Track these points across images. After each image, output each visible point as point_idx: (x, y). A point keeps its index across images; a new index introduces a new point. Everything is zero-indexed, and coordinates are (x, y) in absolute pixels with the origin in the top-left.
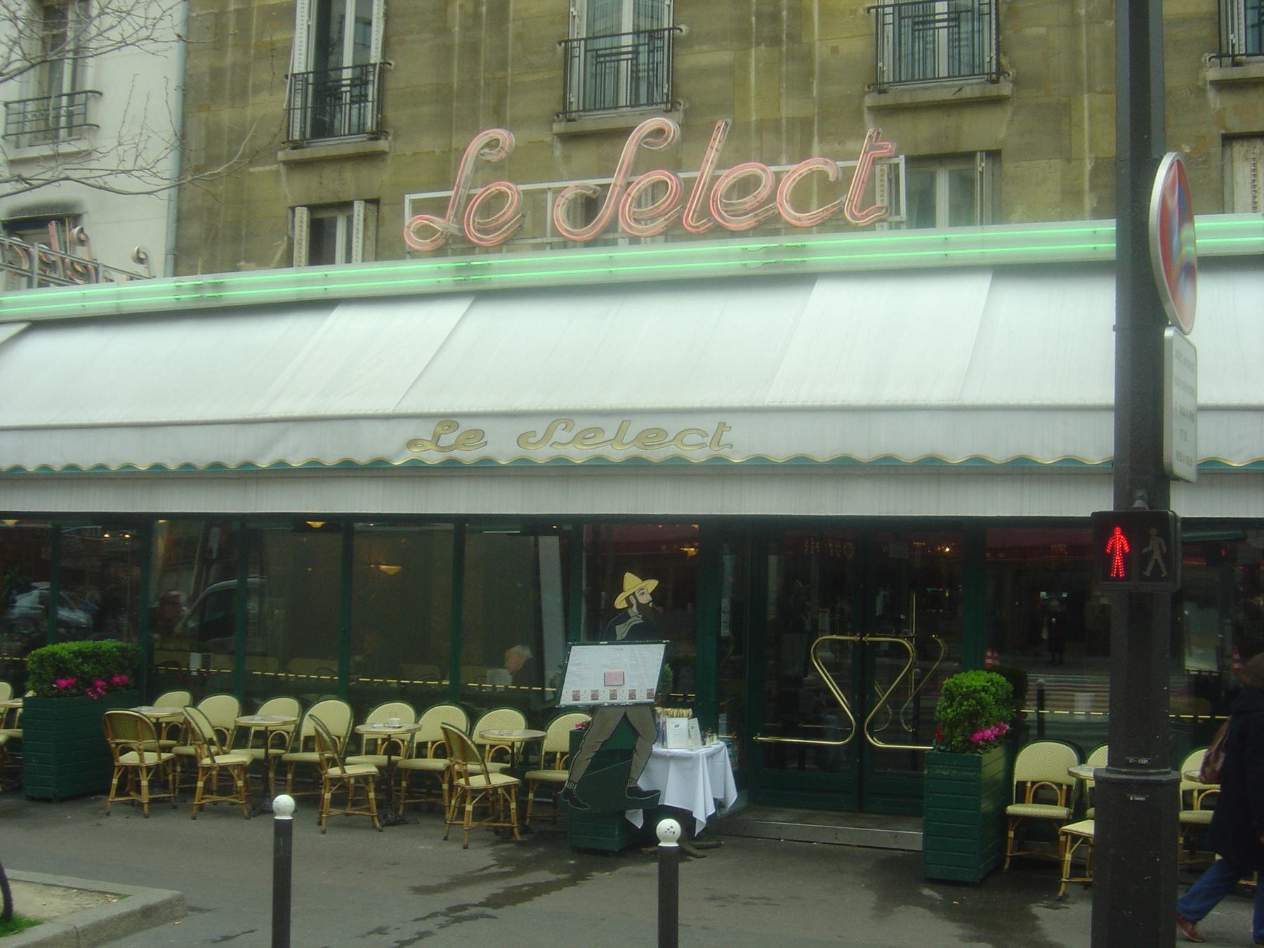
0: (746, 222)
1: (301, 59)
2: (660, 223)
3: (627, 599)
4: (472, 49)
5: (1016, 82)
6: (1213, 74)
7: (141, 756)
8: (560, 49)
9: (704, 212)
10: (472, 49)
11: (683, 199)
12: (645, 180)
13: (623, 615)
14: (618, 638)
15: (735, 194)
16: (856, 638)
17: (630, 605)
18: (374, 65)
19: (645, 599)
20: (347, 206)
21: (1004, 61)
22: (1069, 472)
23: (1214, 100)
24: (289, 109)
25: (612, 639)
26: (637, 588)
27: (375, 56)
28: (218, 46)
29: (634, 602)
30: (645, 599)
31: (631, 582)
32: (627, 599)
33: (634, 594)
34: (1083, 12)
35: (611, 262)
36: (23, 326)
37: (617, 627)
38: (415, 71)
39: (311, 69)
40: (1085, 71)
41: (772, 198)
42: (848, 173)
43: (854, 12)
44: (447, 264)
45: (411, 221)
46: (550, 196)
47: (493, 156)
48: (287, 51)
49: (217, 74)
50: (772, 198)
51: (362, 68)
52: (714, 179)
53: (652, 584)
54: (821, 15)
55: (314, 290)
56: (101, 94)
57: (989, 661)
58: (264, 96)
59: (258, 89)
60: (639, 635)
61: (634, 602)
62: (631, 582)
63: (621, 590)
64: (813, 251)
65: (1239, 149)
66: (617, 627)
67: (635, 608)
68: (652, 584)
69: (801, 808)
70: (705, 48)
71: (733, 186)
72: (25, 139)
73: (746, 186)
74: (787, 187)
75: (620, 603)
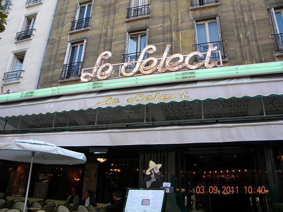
1: (66, 61)
3: (150, 171)
5: (229, 59)
8: (122, 57)
9: (164, 65)
11: (158, 64)
13: (149, 178)
14: (147, 187)
15: (172, 62)
17: (152, 174)
18: (81, 62)
19: (157, 171)
21: (225, 55)
24: (62, 71)
25: (145, 188)
26: (154, 167)
27: (82, 60)
28: (50, 61)
29: (153, 172)
30: (157, 171)
31: (152, 164)
32: (150, 171)
33: (153, 169)
34: (243, 44)
37: (147, 182)
39: (68, 63)
40: (245, 56)
41: (184, 62)
42: (205, 55)
43: (189, 46)
44: (91, 83)
45: (83, 75)
46: (120, 66)
48: (63, 61)
49: (49, 66)
50: (184, 62)
51: (79, 63)
52: (166, 59)
53: (160, 166)
54: (182, 47)
55: (56, 93)
58: (57, 70)
59: (56, 68)
60: (156, 186)
61: (153, 172)
62: (152, 164)
63: (148, 167)
64: (197, 74)
66: (147, 182)
67: (153, 175)
68: (160, 166)
70: (155, 55)
71: (171, 61)
74: (187, 59)
75: (148, 173)
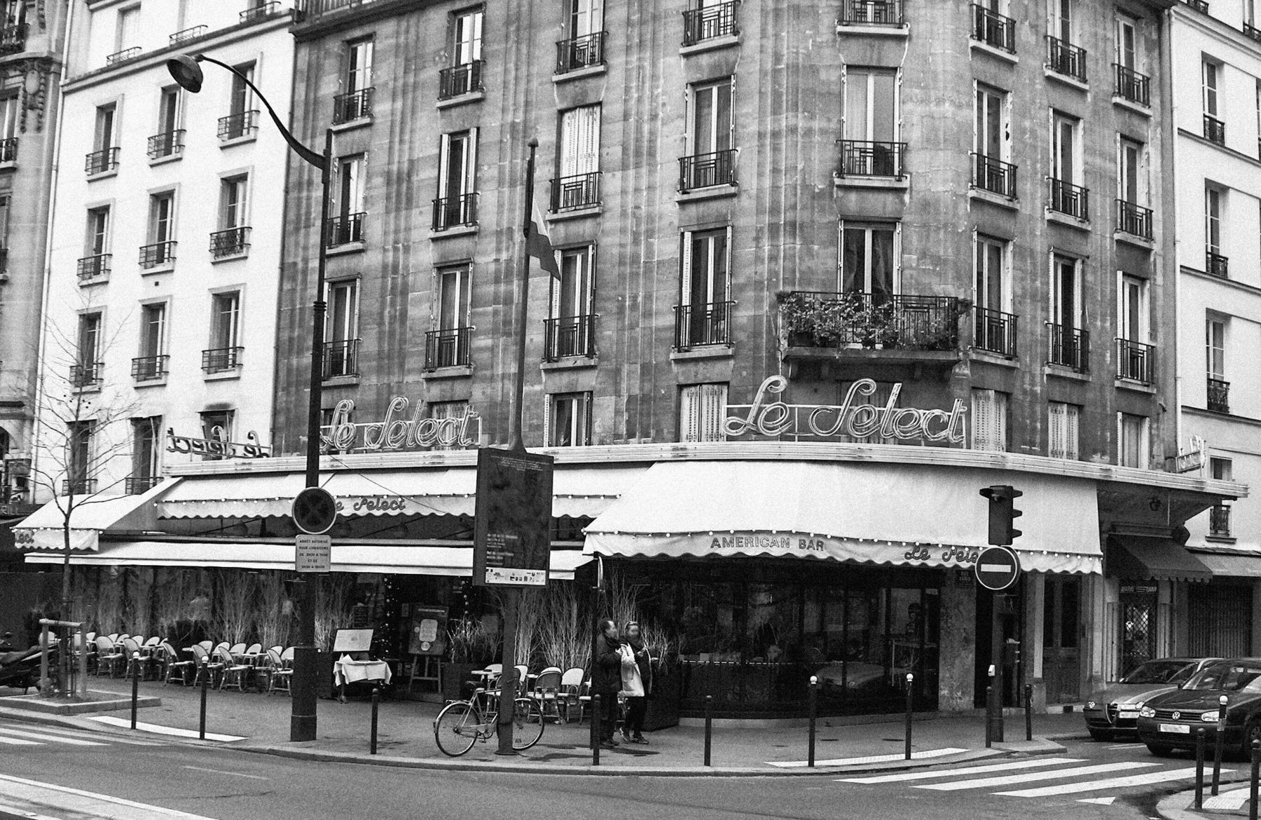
0: (776, 433)
2: (397, 445)
4: (392, 333)
6: (672, 356)
7: (1002, 507)
10: (392, 333)
12: (769, 407)
16: (61, 622)
20: (466, 132)
22: (236, 438)
23: (675, 367)
35: (215, 467)
36: (287, 127)
38: (370, 345)
41: (755, 422)
47: (866, 393)
56: (152, 166)
57: (354, 672)
65: (567, 115)
69: (736, 718)
72: (212, 370)
73: (909, 417)
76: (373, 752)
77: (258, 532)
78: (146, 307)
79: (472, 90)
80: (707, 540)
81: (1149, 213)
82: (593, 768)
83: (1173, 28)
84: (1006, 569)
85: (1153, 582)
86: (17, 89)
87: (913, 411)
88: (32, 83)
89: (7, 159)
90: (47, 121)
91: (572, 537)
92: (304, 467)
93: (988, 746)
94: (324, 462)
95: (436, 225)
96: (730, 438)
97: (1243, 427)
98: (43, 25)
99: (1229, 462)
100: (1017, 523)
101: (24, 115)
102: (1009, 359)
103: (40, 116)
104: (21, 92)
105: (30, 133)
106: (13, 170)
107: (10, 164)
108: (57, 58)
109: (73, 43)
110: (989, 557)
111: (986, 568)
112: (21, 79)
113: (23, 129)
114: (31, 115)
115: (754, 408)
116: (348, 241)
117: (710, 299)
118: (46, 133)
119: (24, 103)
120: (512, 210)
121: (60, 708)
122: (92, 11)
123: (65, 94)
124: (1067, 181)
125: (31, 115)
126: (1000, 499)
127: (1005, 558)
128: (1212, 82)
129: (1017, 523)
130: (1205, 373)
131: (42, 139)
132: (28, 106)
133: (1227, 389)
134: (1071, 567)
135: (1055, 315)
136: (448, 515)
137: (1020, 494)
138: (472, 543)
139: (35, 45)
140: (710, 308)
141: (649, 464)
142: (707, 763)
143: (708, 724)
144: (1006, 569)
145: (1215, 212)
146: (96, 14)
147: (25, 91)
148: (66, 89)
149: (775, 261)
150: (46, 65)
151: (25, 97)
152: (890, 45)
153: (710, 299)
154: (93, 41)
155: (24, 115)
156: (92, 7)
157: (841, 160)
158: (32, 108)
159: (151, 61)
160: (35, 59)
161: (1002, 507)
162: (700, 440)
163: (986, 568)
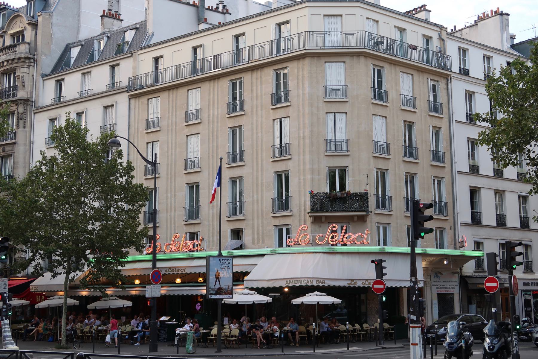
7: (379, 266)
76: (119, 353)
77: (211, 259)
78: (77, 114)
79: (240, 161)
80: (285, 281)
81: (444, 153)
82: (217, 354)
83: (453, 83)
84: (382, 287)
85: (527, 173)
86: (14, 111)
87: (351, 234)
88: (21, 109)
89: (12, 139)
90: (28, 124)
91: (241, 281)
92: (205, 264)
93: (377, 346)
94: (159, 257)
95: (274, 156)
96: (332, 245)
97: (488, 228)
98: (24, 86)
99: (482, 243)
100: (384, 271)
101: (18, 122)
102: (389, 212)
103: (25, 122)
104: (16, 112)
105: (21, 129)
106: (15, 143)
107: (13, 141)
108: (30, 99)
109: (37, 93)
110: (376, 283)
111: (375, 286)
112: (16, 107)
113: (18, 127)
114: (21, 122)
115: (327, 236)
116: (281, 102)
117: (238, 150)
118: (28, 129)
119: (18, 117)
120: (213, 236)
121: (114, 339)
122: (44, 80)
123: (34, 113)
124: (437, 151)
125: (21, 122)
126: (378, 263)
127: (381, 283)
128: (473, 149)
129: (384, 271)
130: (495, 212)
131: (26, 132)
132: (19, 119)
133: (528, 220)
134: (398, 285)
135: (432, 147)
136: (334, 286)
137: (385, 261)
138: (205, 284)
139: (21, 94)
140: (282, 93)
141: (263, 255)
142: (178, 353)
143: (412, 344)
144: (382, 287)
145: (470, 101)
146: (45, 82)
147: (18, 112)
148: (35, 112)
149: (308, 182)
150: (26, 102)
151: (18, 115)
152: (196, 226)
153: (238, 150)
154: (2, 197)
155: (18, 122)
156: (44, 79)
157: (195, 62)
158: (21, 119)
159: (71, 103)
160: (22, 100)
161: (379, 266)
162: (437, 248)
163: (375, 286)
